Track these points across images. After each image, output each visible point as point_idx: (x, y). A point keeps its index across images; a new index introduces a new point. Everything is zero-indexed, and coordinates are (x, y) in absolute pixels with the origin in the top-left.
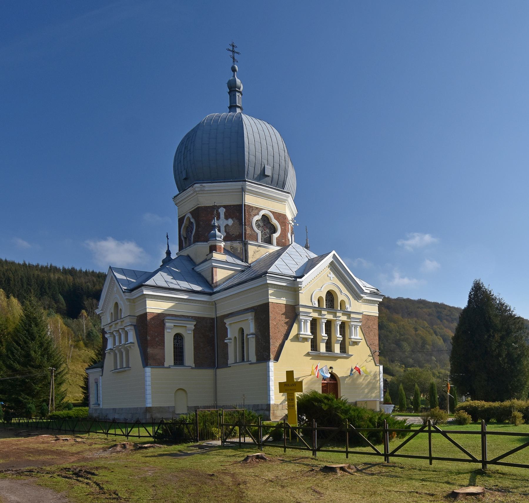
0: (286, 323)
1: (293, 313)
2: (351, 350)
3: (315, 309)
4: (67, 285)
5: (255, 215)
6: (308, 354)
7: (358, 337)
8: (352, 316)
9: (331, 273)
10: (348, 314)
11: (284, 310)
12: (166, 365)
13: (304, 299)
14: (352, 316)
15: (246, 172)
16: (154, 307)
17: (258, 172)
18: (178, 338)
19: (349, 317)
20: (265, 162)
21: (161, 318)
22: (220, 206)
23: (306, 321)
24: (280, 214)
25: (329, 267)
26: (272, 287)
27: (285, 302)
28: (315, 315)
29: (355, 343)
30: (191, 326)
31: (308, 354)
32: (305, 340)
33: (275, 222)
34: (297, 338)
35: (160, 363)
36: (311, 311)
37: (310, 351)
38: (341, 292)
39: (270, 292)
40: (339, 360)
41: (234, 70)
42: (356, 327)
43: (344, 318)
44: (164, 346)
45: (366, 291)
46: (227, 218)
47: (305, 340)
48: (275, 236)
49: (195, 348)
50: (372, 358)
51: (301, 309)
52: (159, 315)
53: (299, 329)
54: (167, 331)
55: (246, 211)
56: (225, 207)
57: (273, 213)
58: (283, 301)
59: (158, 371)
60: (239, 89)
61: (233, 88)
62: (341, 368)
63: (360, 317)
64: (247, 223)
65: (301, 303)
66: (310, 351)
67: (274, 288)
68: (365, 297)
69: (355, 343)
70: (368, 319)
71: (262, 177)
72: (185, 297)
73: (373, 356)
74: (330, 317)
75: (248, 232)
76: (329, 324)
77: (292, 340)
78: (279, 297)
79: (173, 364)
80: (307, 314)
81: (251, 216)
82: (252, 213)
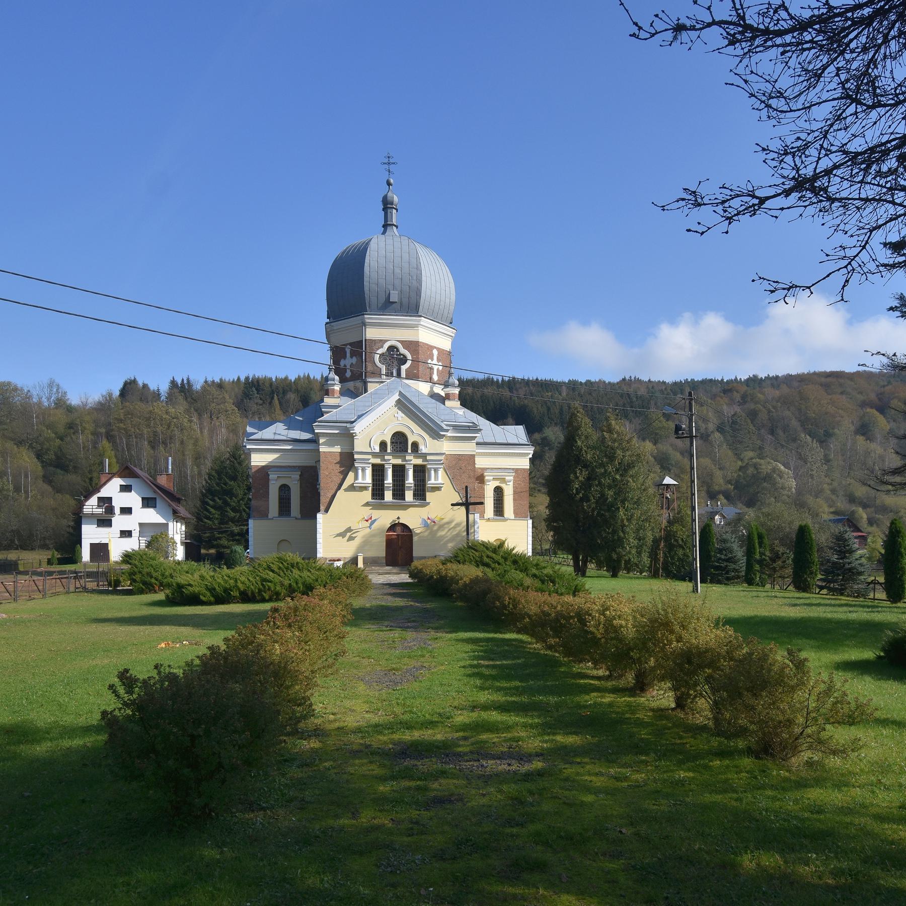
1: (348, 462)
2: (429, 496)
3: (374, 455)
4: (492, 403)
6: (367, 504)
7: (440, 481)
9: (400, 412)
10: (424, 456)
11: (338, 459)
13: (359, 445)
14: (428, 458)
17: (383, 299)
18: (284, 490)
19: (425, 460)
20: (391, 287)
21: (264, 471)
22: (346, 345)
23: (363, 470)
28: (378, 461)
29: (437, 489)
30: (296, 476)
31: (367, 504)
33: (403, 351)
34: (352, 488)
35: (264, 515)
36: (370, 457)
39: (321, 441)
41: (389, 184)
42: (436, 470)
43: (419, 461)
45: (445, 427)
46: (351, 357)
48: (404, 368)
51: (356, 456)
52: (263, 467)
53: (356, 478)
54: (271, 483)
56: (351, 344)
57: (402, 342)
58: (337, 449)
61: (387, 205)
62: (413, 518)
63: (442, 458)
65: (356, 449)
68: (449, 434)
69: (437, 489)
70: (460, 460)
71: (387, 306)
72: (289, 447)
74: (399, 461)
75: (370, 368)
76: (399, 472)
77: (346, 490)
80: (365, 461)
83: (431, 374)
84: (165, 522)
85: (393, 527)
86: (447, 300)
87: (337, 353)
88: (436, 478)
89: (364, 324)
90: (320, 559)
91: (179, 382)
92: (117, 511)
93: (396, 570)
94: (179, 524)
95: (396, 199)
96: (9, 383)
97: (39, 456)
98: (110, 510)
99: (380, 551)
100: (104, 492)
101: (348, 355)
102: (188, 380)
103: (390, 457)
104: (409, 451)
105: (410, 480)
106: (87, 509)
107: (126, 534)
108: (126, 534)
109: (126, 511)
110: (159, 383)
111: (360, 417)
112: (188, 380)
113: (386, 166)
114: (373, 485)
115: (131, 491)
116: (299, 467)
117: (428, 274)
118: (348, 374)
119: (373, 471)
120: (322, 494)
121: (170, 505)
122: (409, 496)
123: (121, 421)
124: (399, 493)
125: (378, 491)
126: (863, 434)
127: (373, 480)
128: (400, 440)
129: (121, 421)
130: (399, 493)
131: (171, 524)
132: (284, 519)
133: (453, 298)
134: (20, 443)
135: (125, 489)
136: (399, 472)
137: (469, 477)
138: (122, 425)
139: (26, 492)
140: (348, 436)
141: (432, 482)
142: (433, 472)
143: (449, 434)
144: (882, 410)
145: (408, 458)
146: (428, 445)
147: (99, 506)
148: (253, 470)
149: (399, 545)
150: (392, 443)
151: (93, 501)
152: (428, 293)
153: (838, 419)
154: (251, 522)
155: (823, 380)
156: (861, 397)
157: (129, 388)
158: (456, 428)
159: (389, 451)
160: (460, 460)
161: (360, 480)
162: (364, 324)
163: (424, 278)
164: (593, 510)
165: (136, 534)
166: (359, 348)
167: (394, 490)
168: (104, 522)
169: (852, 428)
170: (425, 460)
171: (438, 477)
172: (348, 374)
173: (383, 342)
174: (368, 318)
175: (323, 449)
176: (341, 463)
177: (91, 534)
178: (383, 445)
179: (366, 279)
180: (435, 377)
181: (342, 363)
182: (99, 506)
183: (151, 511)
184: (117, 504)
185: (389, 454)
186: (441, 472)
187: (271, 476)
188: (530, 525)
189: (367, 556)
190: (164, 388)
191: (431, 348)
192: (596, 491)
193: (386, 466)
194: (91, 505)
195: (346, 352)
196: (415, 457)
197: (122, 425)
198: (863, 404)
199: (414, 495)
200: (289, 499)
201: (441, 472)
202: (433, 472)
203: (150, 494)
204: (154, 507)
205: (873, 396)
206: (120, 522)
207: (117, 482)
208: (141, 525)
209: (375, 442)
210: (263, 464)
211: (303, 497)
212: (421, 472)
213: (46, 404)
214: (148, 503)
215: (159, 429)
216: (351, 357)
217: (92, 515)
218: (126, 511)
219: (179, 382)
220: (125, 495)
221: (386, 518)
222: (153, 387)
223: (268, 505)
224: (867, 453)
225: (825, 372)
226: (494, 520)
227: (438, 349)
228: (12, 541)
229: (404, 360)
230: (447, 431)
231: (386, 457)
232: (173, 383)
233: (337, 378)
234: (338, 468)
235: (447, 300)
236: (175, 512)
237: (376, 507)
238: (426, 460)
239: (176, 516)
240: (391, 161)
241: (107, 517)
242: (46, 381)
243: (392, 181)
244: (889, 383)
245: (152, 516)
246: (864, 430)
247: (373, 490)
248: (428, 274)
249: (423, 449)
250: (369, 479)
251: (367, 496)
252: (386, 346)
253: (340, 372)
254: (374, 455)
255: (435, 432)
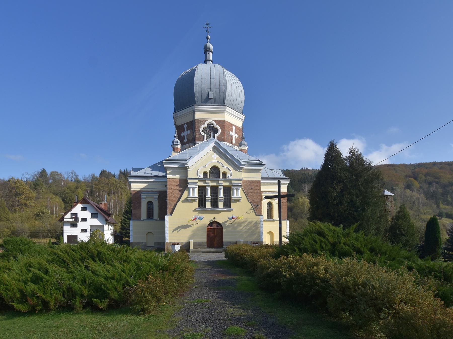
0: (180, 191)
1: (184, 184)
2: (233, 205)
3: (200, 180)
5: (202, 125)
6: (196, 210)
7: (239, 196)
8: (233, 182)
9: (215, 154)
11: (178, 183)
12: (142, 219)
15: (196, 100)
16: (136, 187)
17: (204, 97)
18: (150, 204)
19: (231, 183)
20: (209, 90)
21: (138, 194)
22: (184, 124)
23: (193, 189)
24: (220, 121)
25: (213, 150)
26: (169, 169)
27: (179, 178)
28: (202, 184)
29: (238, 200)
30: (156, 196)
31: (196, 210)
32: (194, 200)
34: (187, 200)
35: (138, 218)
36: (197, 181)
37: (197, 207)
38: (223, 166)
40: (222, 213)
41: (208, 39)
42: (237, 189)
43: (227, 184)
44: (141, 209)
45: (243, 163)
46: (187, 130)
47: (194, 200)
48: (217, 135)
49: (159, 209)
50: (253, 210)
51: (189, 181)
52: (138, 191)
53: (189, 194)
54: (142, 200)
55: (196, 125)
56: (187, 123)
57: (215, 121)
58: (178, 177)
59: (138, 223)
60: (209, 49)
63: (241, 182)
64: (196, 131)
65: (189, 176)
66: (197, 207)
67: (171, 169)
68: (245, 167)
69: (238, 200)
70: (251, 183)
71: (207, 100)
73: (253, 209)
74: (214, 184)
75: (197, 136)
76: (215, 190)
77: (183, 202)
78: (175, 174)
79: (146, 218)
80: (194, 184)
81: (199, 126)
82: (200, 124)
83: (232, 139)
84: (101, 224)
85: (211, 224)
86: (240, 99)
87: (180, 129)
88: (237, 194)
89: (194, 111)
90: (167, 243)
91: (123, 171)
92: (80, 220)
93: (213, 250)
94: (110, 226)
95: (212, 47)
96: (55, 172)
97: (63, 200)
98: (76, 219)
99: (203, 239)
100: (74, 211)
101: (186, 129)
102: (126, 170)
103: (209, 181)
104: (221, 178)
105: (221, 195)
106: (66, 219)
107: (84, 230)
108: (84, 230)
109: (84, 220)
110: (116, 172)
111: (190, 157)
112: (126, 170)
113: (206, 29)
114: (199, 199)
115: (86, 210)
116: (158, 191)
117: (230, 83)
118: (186, 140)
119: (199, 190)
120: (168, 203)
121: (104, 217)
122: (221, 205)
123: (96, 185)
124: (215, 203)
125: (202, 202)
126: (409, 188)
127: (199, 195)
128: (215, 170)
129: (96, 185)
130: (215, 203)
131: (105, 226)
132: (150, 221)
133: (243, 104)
134: (56, 194)
135: (84, 209)
136: (215, 190)
137: (257, 194)
138: (97, 187)
139: (56, 214)
140: (184, 169)
141: (235, 196)
142: (235, 191)
143: (245, 167)
144: (415, 178)
145: (220, 182)
146: (232, 174)
147: (71, 217)
148: (133, 193)
149: (215, 234)
150: (210, 173)
151: (69, 215)
152: (230, 93)
153: (397, 182)
154: (131, 222)
155: (387, 167)
156: (404, 174)
157: (103, 173)
158: (250, 164)
159: (209, 177)
160: (251, 183)
161: (191, 195)
162: (194, 111)
163: (228, 85)
164: (345, 211)
165: (88, 230)
166: (192, 125)
167: (211, 202)
168: (74, 225)
169: (404, 186)
170: (231, 183)
171: (238, 194)
172: (186, 140)
173: (205, 121)
174: (197, 107)
175: (169, 177)
176: (180, 185)
177: (68, 231)
178: (205, 174)
179: (195, 85)
180: (234, 142)
181: (182, 135)
182: (71, 217)
183: (96, 220)
184: (80, 217)
185: (209, 179)
186: (240, 190)
187: (142, 197)
188: (288, 224)
189: (195, 241)
190: (117, 173)
191: (232, 125)
192: (348, 198)
193: (207, 187)
194: (68, 217)
195: (184, 128)
196: (225, 181)
197: (97, 187)
198: (407, 176)
199: (224, 205)
200: (153, 209)
201: (240, 190)
202: (235, 191)
203: (95, 212)
204: (97, 218)
205: (410, 173)
206: (81, 225)
207: (80, 206)
208: (91, 226)
209: (200, 172)
210: (138, 190)
211: (160, 209)
212: (228, 190)
213: (70, 180)
214: (94, 216)
215: (112, 188)
216: (187, 130)
217: (68, 222)
218: (84, 220)
219: (123, 171)
220: (84, 212)
221: (207, 218)
222: (113, 173)
223: (141, 213)
224: (411, 196)
225: (387, 165)
226: (267, 221)
227: (236, 126)
228: (48, 234)
229: (216, 131)
230: (244, 165)
231: (207, 182)
232: (121, 171)
233: (179, 141)
234: (178, 188)
235: (240, 99)
236: (107, 220)
237: (200, 212)
238: (231, 183)
239: (107, 222)
240: (209, 26)
241: (75, 222)
242: (70, 171)
243: (209, 37)
244: (415, 168)
245: (96, 222)
246: (409, 186)
247: (199, 202)
248: (230, 83)
249: (229, 176)
250: (196, 195)
251: (195, 205)
252: (207, 123)
253: (180, 138)
254: (200, 180)
255: (237, 166)
